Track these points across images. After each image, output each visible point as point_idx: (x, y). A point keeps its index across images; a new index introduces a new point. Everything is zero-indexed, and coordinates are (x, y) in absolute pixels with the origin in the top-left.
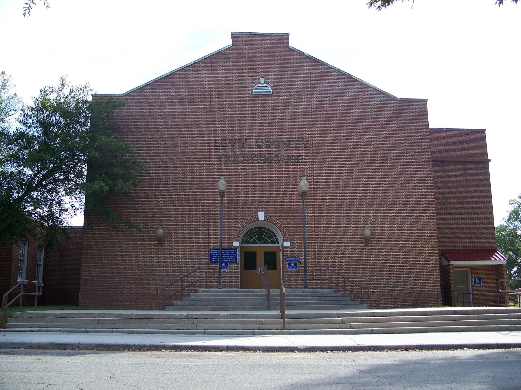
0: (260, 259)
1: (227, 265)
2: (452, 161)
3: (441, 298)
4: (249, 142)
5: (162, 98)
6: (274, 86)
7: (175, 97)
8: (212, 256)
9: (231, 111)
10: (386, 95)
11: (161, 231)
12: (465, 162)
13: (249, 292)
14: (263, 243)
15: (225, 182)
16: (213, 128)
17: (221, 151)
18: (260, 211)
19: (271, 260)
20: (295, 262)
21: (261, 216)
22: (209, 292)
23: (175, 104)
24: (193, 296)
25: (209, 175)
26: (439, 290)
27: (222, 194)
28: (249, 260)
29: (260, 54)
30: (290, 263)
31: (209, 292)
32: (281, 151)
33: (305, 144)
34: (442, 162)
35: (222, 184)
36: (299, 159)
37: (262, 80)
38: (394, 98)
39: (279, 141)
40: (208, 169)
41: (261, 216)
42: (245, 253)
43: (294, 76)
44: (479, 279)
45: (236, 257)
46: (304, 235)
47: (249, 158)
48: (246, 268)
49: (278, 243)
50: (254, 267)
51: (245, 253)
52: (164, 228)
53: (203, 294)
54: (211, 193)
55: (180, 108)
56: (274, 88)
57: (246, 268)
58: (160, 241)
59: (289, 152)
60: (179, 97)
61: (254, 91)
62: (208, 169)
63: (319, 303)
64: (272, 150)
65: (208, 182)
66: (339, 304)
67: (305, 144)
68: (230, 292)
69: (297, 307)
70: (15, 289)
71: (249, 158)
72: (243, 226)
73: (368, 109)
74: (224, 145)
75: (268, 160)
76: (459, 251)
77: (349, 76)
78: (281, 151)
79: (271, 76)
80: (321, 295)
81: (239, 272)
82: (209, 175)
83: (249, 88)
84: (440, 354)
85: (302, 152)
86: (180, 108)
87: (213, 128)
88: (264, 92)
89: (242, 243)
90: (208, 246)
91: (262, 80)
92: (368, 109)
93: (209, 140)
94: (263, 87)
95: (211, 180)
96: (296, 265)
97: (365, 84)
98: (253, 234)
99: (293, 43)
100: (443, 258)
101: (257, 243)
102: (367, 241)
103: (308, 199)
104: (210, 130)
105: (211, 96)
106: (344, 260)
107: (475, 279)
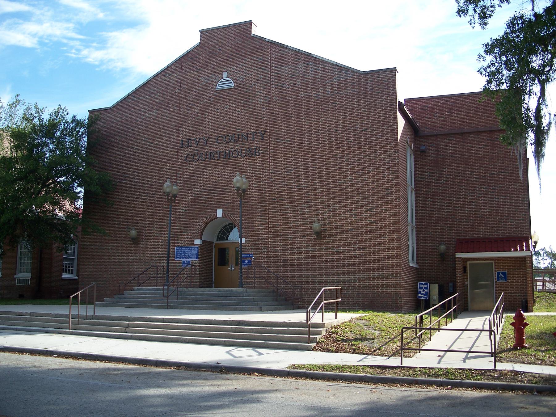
2: (474, 132)
9: (197, 110)
10: (348, 70)
11: (133, 233)
12: (491, 131)
16: (180, 129)
17: (187, 151)
18: (219, 208)
22: (142, 290)
24: (126, 294)
31: (142, 290)
32: (240, 146)
34: (462, 134)
36: (256, 152)
37: (225, 75)
38: (357, 72)
42: (219, 249)
43: (255, 65)
44: (504, 274)
47: (211, 156)
51: (219, 249)
53: (136, 292)
55: (155, 113)
56: (235, 81)
58: (136, 241)
59: (247, 146)
60: (154, 103)
61: (218, 87)
64: (232, 145)
69: (196, 307)
71: (211, 156)
73: (328, 89)
74: (190, 145)
75: (227, 156)
76: (473, 241)
77: (309, 55)
78: (240, 146)
79: (233, 69)
83: (213, 84)
84: (28, 359)
85: (260, 144)
86: (155, 113)
87: (180, 129)
88: (225, 87)
91: (225, 75)
93: (178, 141)
94: (226, 82)
96: (249, 262)
97: (326, 62)
99: (256, 31)
102: (319, 235)
104: (179, 132)
105: (180, 98)
107: (499, 273)
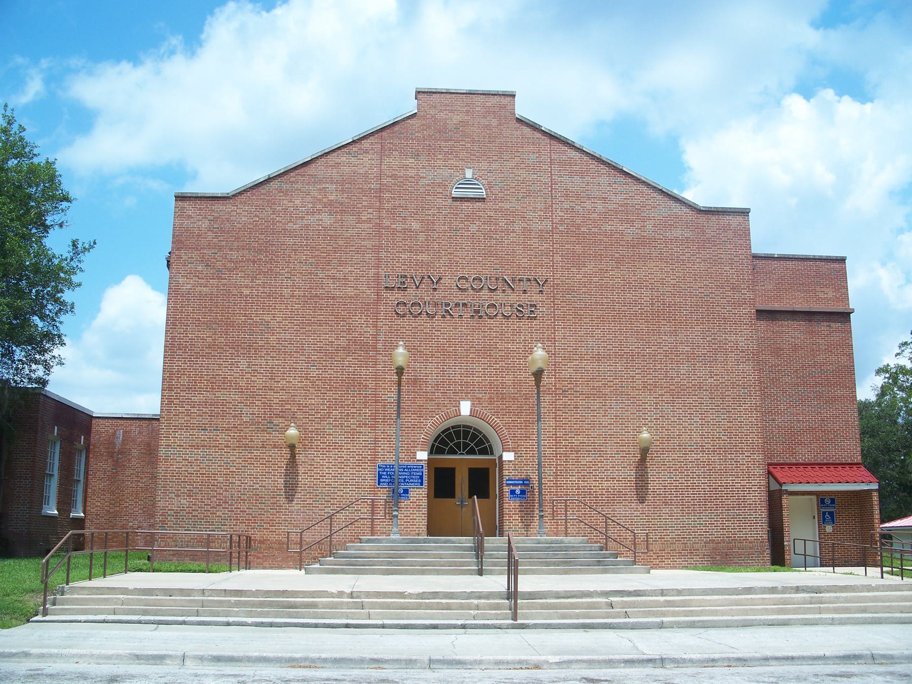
0: (462, 481)
1: (406, 491)
3: (768, 551)
4: (445, 281)
5: (297, 202)
6: (489, 183)
7: (320, 200)
8: (380, 477)
9: (415, 226)
13: (446, 542)
14: (467, 453)
15: (405, 351)
16: (383, 254)
17: (398, 296)
18: (463, 399)
19: (481, 482)
20: (523, 488)
21: (465, 408)
22: (379, 541)
23: (319, 212)
24: (353, 549)
25: (375, 336)
26: (765, 537)
27: (400, 371)
28: (442, 483)
29: (463, 123)
30: (514, 488)
31: (379, 541)
33: (541, 284)
35: (401, 354)
39: (497, 279)
40: (376, 326)
41: (465, 408)
44: (831, 514)
45: (421, 477)
46: (538, 442)
48: (436, 496)
49: (492, 453)
50: (452, 495)
52: (298, 427)
54: (380, 367)
55: (327, 219)
57: (436, 496)
60: (325, 200)
62: (376, 326)
63: (566, 562)
65: (375, 347)
66: (599, 563)
67: (541, 284)
68: (413, 541)
70: (132, 599)
72: (432, 426)
73: (649, 226)
79: (484, 165)
80: (567, 549)
81: (424, 503)
82: (375, 336)
85: (537, 298)
86: (327, 219)
87: (383, 254)
89: (431, 453)
90: (374, 460)
92: (649, 226)
95: (380, 346)
98: (449, 436)
100: (771, 479)
101: (455, 453)
103: (545, 380)
105: (380, 199)
106: (605, 484)
